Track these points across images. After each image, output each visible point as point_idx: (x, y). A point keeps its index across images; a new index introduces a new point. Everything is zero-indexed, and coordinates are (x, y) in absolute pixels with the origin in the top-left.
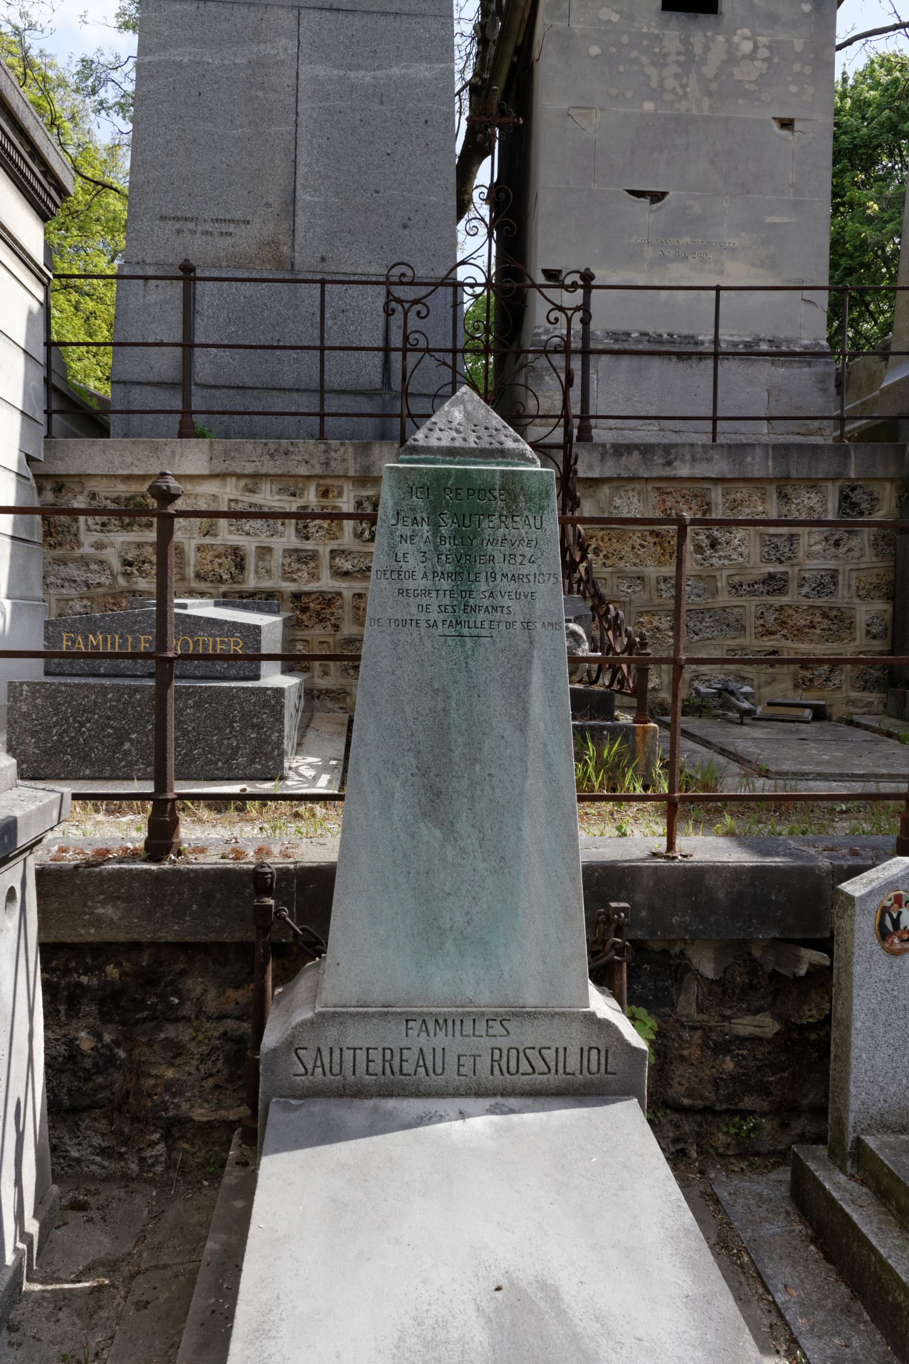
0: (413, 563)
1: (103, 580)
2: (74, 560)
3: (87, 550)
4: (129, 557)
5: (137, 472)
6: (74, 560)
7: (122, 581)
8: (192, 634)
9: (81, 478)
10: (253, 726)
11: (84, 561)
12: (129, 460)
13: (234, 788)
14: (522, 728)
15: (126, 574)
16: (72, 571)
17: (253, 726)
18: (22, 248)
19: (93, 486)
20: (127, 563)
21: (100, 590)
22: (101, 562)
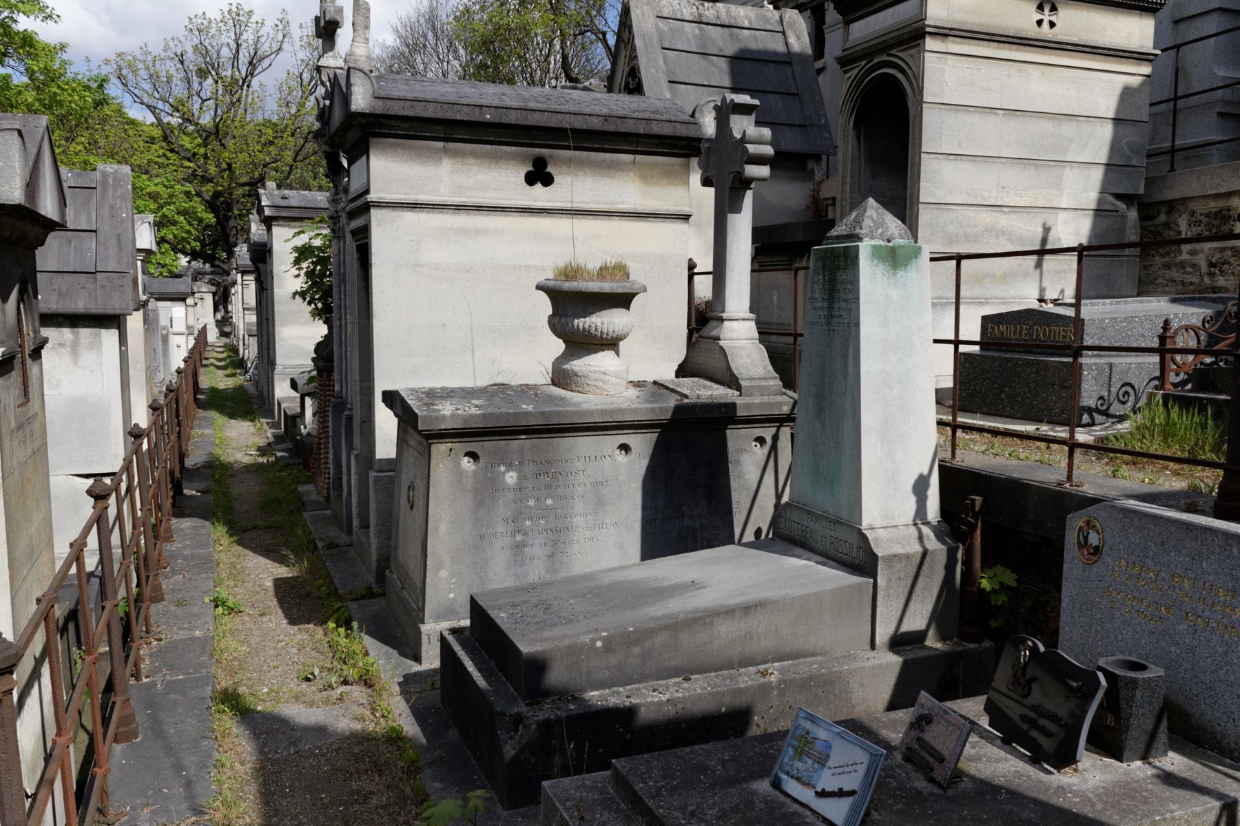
0: (818, 296)
1: (1194, 280)
2: (1176, 265)
3: (1185, 256)
4: (1214, 260)
5: (1222, 190)
6: (1176, 265)
7: (1207, 280)
8: (1048, 325)
9: (1185, 200)
10: (1065, 388)
11: (1182, 265)
12: (1216, 181)
13: (1029, 428)
14: (845, 377)
15: (1211, 275)
16: (1174, 273)
17: (1065, 388)
18: (1104, 49)
19: (1193, 205)
20: (1212, 265)
21: (1192, 287)
22: (1194, 266)
